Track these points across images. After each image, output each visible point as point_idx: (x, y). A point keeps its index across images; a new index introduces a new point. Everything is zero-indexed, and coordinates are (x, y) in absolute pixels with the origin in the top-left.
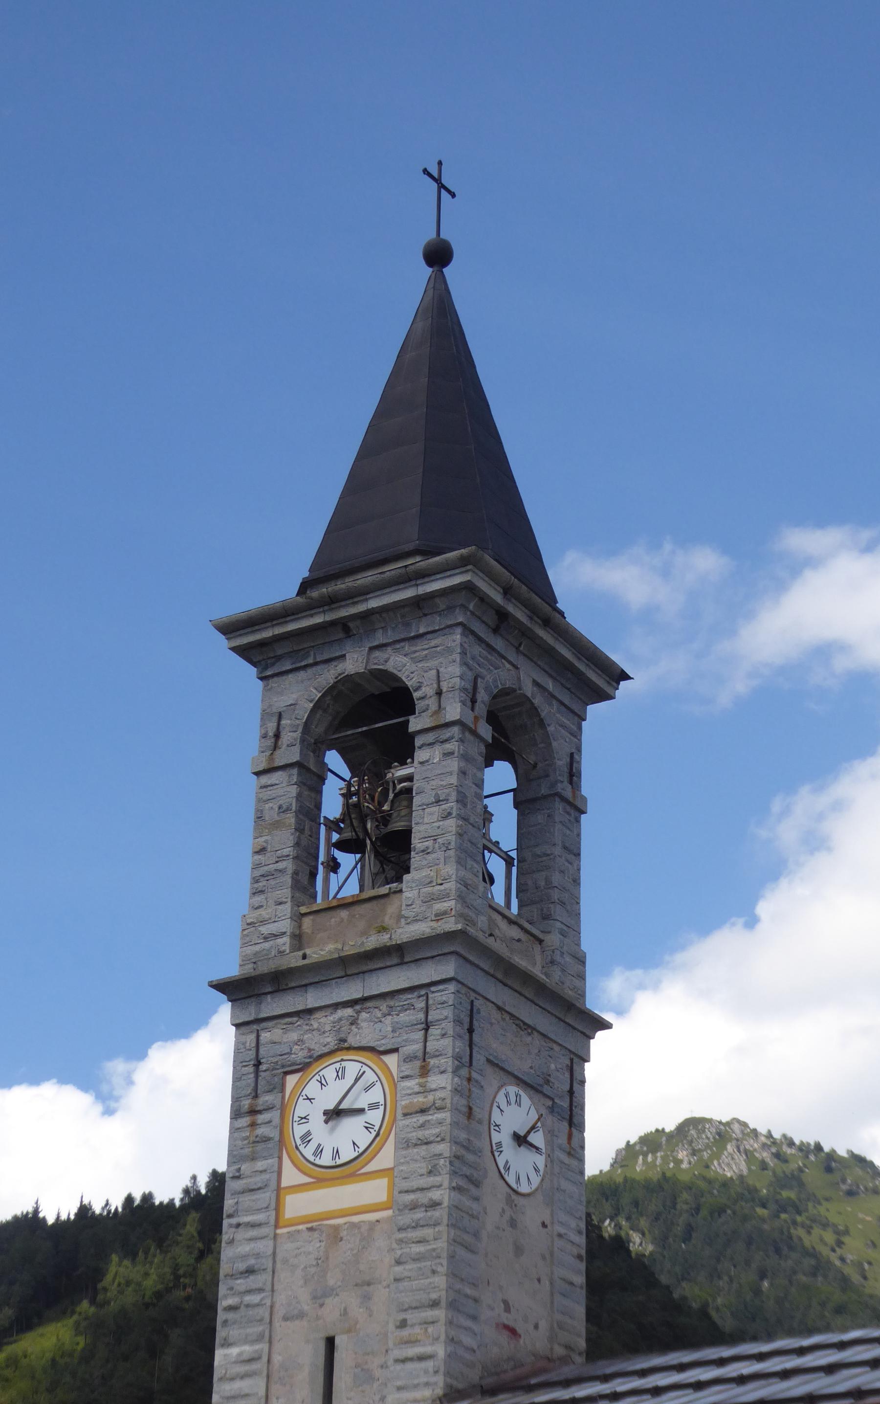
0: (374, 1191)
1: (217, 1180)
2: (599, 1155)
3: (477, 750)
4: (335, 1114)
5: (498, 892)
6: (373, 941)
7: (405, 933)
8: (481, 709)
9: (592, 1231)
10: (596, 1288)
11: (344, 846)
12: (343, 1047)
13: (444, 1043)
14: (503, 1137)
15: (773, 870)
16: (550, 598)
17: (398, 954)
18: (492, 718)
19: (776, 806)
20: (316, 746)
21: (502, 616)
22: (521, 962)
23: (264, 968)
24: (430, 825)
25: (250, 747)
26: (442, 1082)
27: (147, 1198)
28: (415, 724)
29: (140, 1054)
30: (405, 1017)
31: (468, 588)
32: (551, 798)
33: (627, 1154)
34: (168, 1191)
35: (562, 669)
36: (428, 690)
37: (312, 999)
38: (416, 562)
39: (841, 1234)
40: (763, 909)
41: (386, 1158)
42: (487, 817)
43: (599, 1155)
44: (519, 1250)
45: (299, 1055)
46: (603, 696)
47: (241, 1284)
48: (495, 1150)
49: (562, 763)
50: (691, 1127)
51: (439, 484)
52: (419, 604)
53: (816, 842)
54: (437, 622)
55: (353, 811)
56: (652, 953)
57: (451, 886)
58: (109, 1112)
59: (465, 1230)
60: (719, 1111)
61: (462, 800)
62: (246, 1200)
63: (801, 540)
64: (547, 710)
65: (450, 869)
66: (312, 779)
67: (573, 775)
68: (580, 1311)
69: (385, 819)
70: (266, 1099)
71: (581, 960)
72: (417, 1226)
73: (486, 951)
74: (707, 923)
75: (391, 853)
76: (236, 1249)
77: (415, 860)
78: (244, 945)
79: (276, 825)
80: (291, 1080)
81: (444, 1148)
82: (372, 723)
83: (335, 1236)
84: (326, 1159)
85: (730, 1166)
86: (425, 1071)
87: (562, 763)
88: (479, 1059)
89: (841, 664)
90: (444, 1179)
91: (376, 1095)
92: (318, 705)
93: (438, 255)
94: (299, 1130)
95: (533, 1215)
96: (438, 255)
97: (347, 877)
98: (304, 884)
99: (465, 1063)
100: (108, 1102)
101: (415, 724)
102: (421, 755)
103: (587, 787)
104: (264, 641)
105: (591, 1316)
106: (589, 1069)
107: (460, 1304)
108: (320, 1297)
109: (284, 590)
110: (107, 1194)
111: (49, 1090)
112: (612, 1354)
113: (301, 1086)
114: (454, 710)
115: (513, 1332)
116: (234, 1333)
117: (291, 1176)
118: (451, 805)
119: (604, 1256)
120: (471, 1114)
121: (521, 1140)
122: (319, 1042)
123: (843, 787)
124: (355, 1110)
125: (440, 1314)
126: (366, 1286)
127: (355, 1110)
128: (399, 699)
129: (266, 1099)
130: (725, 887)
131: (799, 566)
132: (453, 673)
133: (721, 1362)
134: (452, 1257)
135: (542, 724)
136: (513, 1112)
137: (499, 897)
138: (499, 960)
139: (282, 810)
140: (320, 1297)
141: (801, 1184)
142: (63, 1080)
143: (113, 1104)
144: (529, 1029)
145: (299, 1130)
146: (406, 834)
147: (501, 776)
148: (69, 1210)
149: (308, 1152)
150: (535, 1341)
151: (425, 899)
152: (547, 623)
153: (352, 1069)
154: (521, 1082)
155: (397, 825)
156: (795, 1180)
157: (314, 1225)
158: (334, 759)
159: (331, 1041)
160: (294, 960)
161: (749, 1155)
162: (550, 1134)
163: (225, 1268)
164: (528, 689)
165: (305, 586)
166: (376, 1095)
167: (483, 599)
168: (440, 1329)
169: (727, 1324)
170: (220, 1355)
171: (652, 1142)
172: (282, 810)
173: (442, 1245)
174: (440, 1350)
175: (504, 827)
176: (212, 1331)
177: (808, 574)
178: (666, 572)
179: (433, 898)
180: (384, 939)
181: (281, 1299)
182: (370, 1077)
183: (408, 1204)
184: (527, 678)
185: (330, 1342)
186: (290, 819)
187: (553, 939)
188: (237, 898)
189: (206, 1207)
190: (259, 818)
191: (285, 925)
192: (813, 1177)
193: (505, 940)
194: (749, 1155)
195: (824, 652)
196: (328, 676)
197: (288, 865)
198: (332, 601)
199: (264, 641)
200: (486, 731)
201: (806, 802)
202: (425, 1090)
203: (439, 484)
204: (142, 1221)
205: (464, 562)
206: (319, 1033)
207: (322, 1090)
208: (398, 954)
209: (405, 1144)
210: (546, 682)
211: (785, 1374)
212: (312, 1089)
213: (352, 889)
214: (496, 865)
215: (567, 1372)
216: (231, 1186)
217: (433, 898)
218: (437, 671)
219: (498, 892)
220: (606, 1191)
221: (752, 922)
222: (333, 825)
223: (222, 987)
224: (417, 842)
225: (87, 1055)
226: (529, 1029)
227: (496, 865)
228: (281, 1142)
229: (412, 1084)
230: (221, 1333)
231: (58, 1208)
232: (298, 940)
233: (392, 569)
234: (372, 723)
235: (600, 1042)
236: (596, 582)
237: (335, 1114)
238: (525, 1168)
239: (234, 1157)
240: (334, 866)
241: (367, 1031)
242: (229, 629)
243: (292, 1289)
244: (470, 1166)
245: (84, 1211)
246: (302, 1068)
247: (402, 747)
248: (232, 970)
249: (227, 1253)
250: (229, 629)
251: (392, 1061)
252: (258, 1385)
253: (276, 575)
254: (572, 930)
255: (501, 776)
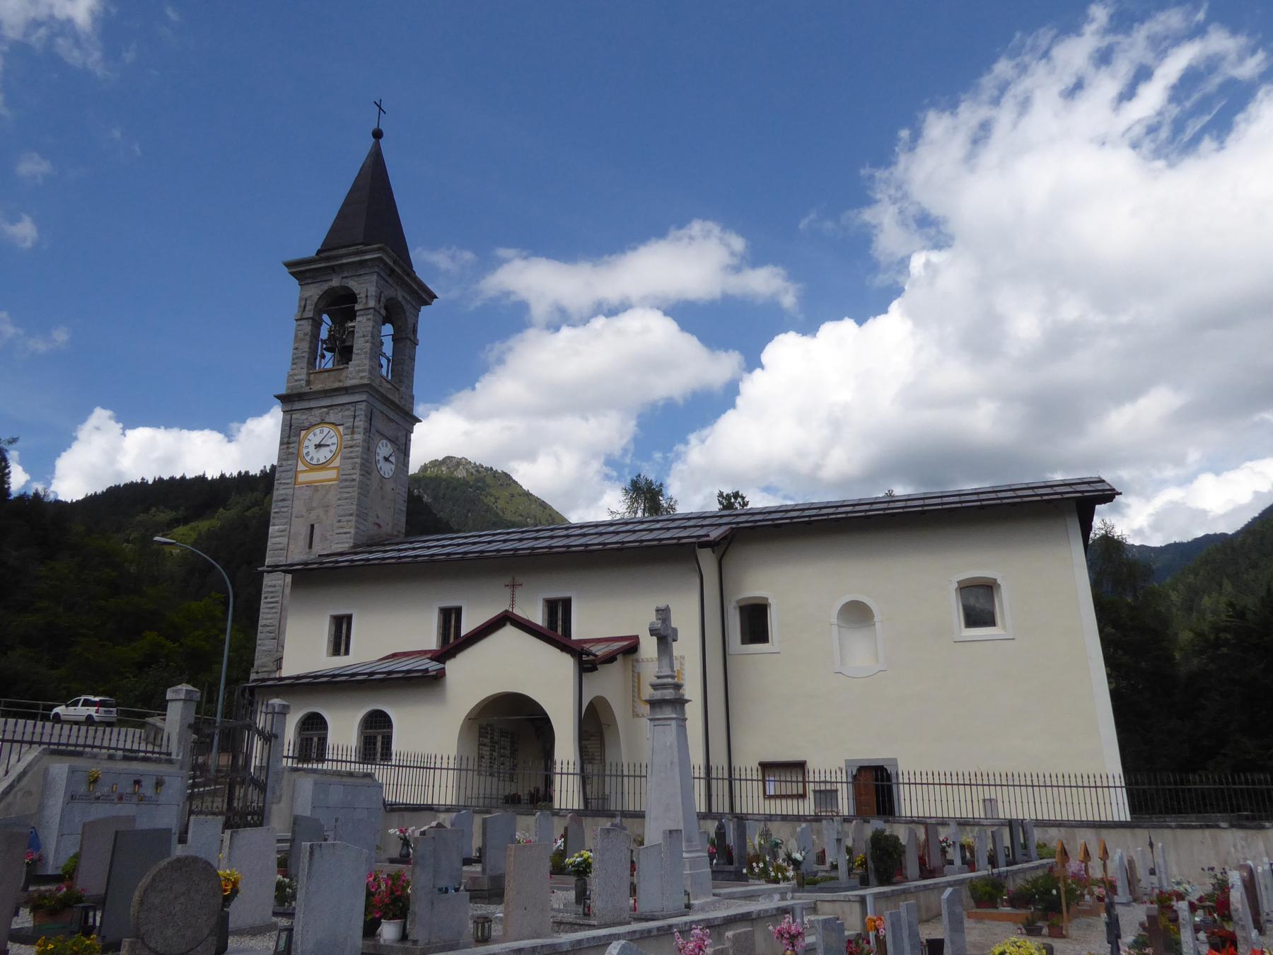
0: (332, 474)
1: (273, 467)
2: (414, 468)
3: (380, 319)
4: (318, 446)
5: (384, 372)
6: (336, 385)
7: (349, 383)
8: (382, 304)
9: (410, 493)
10: (409, 514)
11: (328, 350)
12: (323, 422)
13: (361, 423)
14: (380, 458)
15: (484, 369)
16: (410, 266)
17: (346, 390)
18: (386, 308)
19: (488, 347)
20: (319, 312)
21: (393, 271)
22: (391, 397)
23: (295, 392)
24: (361, 345)
25: (295, 311)
26: (359, 437)
27: (247, 473)
28: (357, 307)
29: (244, 422)
30: (347, 413)
31: (380, 259)
32: (406, 339)
33: (424, 468)
34: (255, 470)
35: (412, 292)
36: (363, 295)
37: (313, 404)
38: (361, 247)
39: (497, 499)
40: (478, 385)
41: (337, 463)
42: (382, 343)
43: (414, 468)
44: (383, 498)
45: (307, 424)
46: (427, 303)
47: (280, 504)
48: (377, 462)
49: (411, 326)
50: (448, 459)
51: (371, 219)
52: (362, 264)
53: (501, 361)
54: (368, 271)
55: (331, 337)
56: (440, 398)
57: (367, 367)
58: (230, 441)
59: (364, 490)
60: (458, 455)
61: (373, 337)
62: (284, 475)
63: (502, 252)
64: (407, 307)
65: (367, 361)
66: (317, 324)
67: (415, 331)
68: (404, 519)
69: (344, 341)
70: (293, 439)
71: (413, 397)
72: (347, 487)
73: (377, 391)
74: (460, 388)
75: (345, 354)
76: (278, 492)
77: (354, 356)
78: (288, 381)
79: (302, 340)
80: (303, 433)
81: (358, 460)
82: (341, 306)
83: (316, 489)
84: (314, 462)
85: (461, 473)
86: (353, 433)
87: (411, 326)
88: (373, 430)
89: (513, 298)
90: (358, 471)
91: (334, 440)
92: (321, 297)
93: (378, 134)
94: (305, 451)
95: (389, 486)
96: (378, 134)
97: (328, 361)
98: (312, 362)
99: (368, 431)
100: (230, 438)
101: (357, 307)
102: (358, 319)
103: (419, 336)
104: (302, 271)
105: (407, 522)
106: (412, 436)
107: (361, 515)
108: (310, 510)
109: (313, 254)
110: (232, 471)
111: (207, 432)
112: (414, 535)
113: (307, 435)
114: (372, 304)
115: (379, 526)
116: (276, 521)
117: (301, 467)
118: (369, 338)
119: (414, 502)
120: (369, 450)
121: (386, 459)
122: (313, 420)
123: (511, 343)
124: (325, 445)
125: (353, 518)
126: (326, 507)
127: (325, 445)
128: (351, 297)
129: (293, 439)
130: (465, 375)
131: (501, 262)
132: (372, 290)
133: (452, 539)
134: (359, 499)
135: (404, 312)
136: (384, 449)
137: (384, 373)
138: (382, 395)
139: (305, 334)
140: (310, 510)
141: (484, 482)
142: (212, 429)
143: (247, 796)
144: (392, 420)
145: (305, 451)
146: (352, 347)
147: (388, 329)
148: (217, 475)
149: (308, 459)
150: (387, 529)
151: (357, 371)
152: (409, 275)
153: (326, 430)
154: (387, 438)
155: (348, 344)
156: (482, 480)
157: (309, 485)
158: (325, 317)
159: (319, 420)
160: (307, 390)
161: (467, 470)
162: (397, 459)
163: (275, 498)
164: (400, 299)
165: (319, 252)
166: (334, 440)
167: (386, 264)
168: (353, 524)
169: (456, 528)
170: (271, 529)
171: (435, 463)
172: (305, 334)
173: (355, 494)
174: (353, 531)
175: (388, 348)
176: (268, 521)
177: (505, 265)
178: (453, 258)
179: (359, 371)
180: (341, 384)
181: (295, 510)
182: (332, 433)
183: (343, 480)
184: (400, 294)
185: (312, 526)
186: (308, 338)
187: (403, 389)
188: (287, 366)
189: (266, 480)
190: (296, 336)
191: (304, 377)
192: (489, 481)
193: (385, 388)
194: (467, 470)
195: (508, 294)
196: (325, 286)
197: (306, 355)
198: (328, 259)
199: (302, 271)
200: (383, 312)
201: (498, 346)
202: (352, 440)
203: (371, 219)
204: (244, 481)
205: (379, 249)
206: (314, 416)
207: (315, 436)
208: (346, 390)
209: (344, 458)
210: (407, 297)
211: (474, 543)
212: (311, 436)
213: (330, 366)
214: (384, 362)
215: (398, 540)
216: (278, 469)
217: (359, 371)
218: (366, 288)
219: (384, 372)
220: (416, 479)
221: (474, 389)
222: (324, 342)
223: (278, 397)
224: (355, 351)
225: (224, 419)
226: (392, 420)
227: (384, 362)
228: (298, 455)
229: (348, 437)
230: (272, 521)
231: (212, 473)
232: (308, 382)
233: (353, 249)
234: (341, 306)
235: (417, 427)
236: (431, 260)
237: (318, 446)
238: (387, 469)
239: (280, 459)
240: (323, 356)
241: (332, 417)
242: (289, 265)
243: (299, 506)
244: (367, 467)
245: (222, 476)
246: (308, 428)
247: (352, 316)
248: (283, 391)
249: (275, 493)
250: (289, 265)
251: (341, 428)
252: (285, 540)
253: (309, 245)
254: (410, 387)
255: (388, 329)
